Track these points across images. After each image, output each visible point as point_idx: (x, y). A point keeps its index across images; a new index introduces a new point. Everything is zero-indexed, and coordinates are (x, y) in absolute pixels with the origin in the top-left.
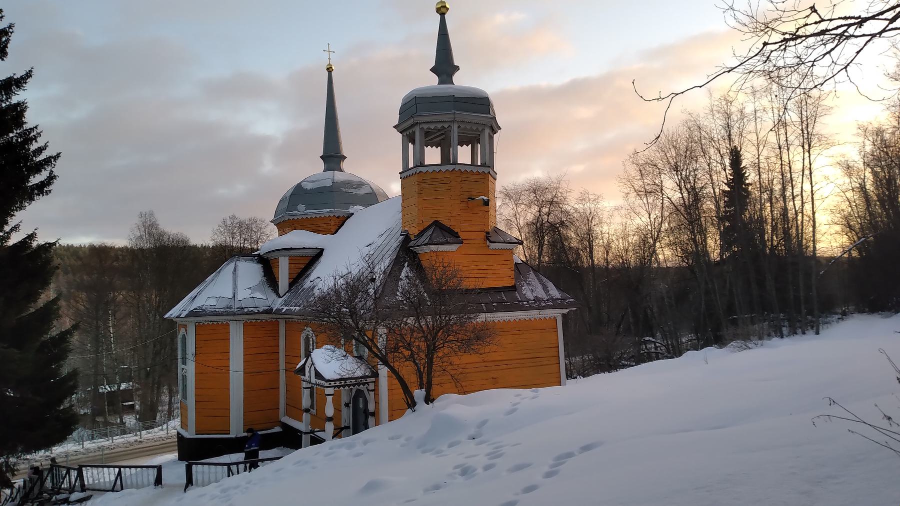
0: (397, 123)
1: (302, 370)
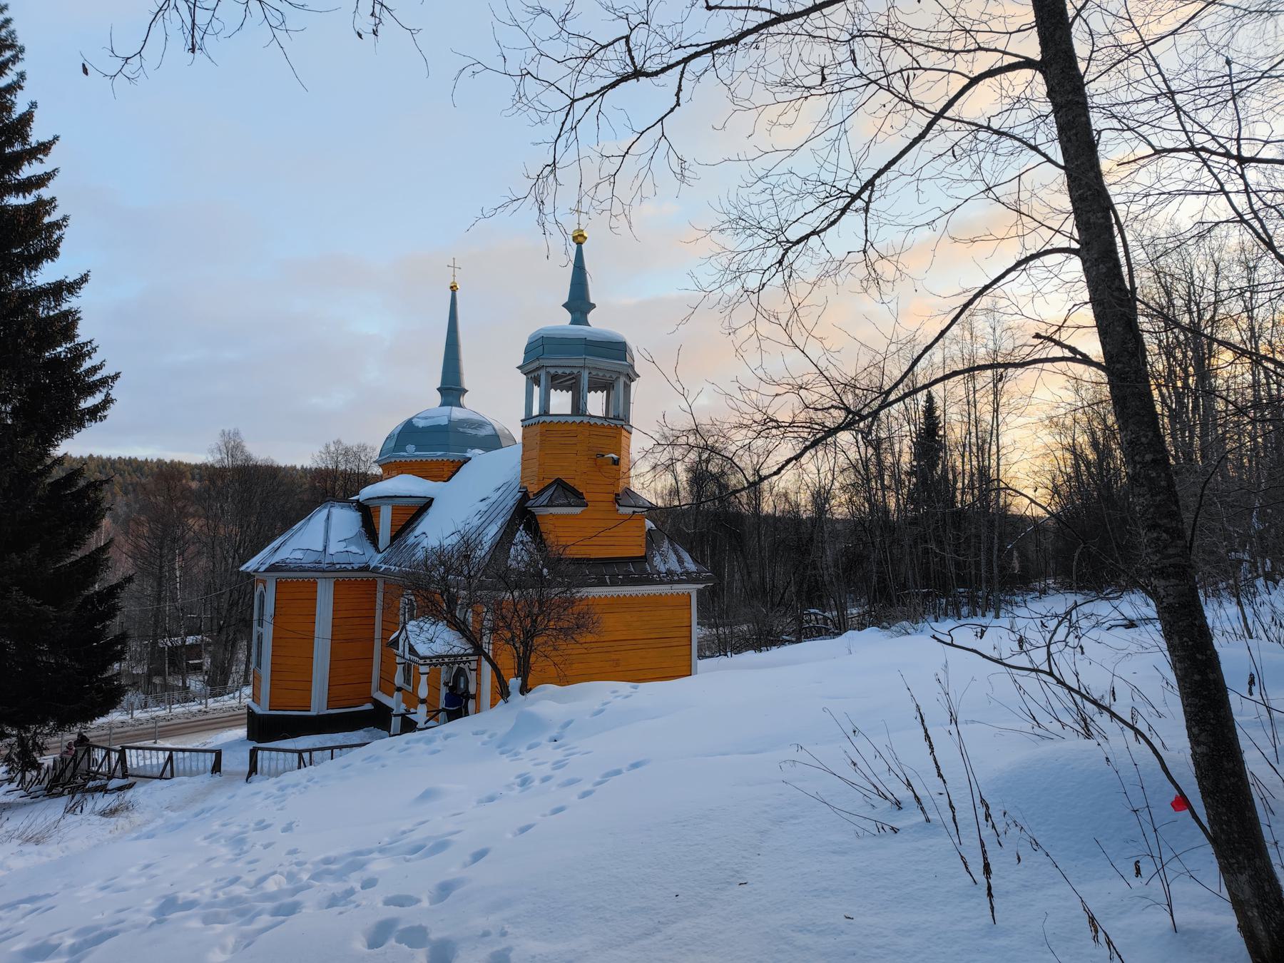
0: (520, 362)
1: (395, 643)
